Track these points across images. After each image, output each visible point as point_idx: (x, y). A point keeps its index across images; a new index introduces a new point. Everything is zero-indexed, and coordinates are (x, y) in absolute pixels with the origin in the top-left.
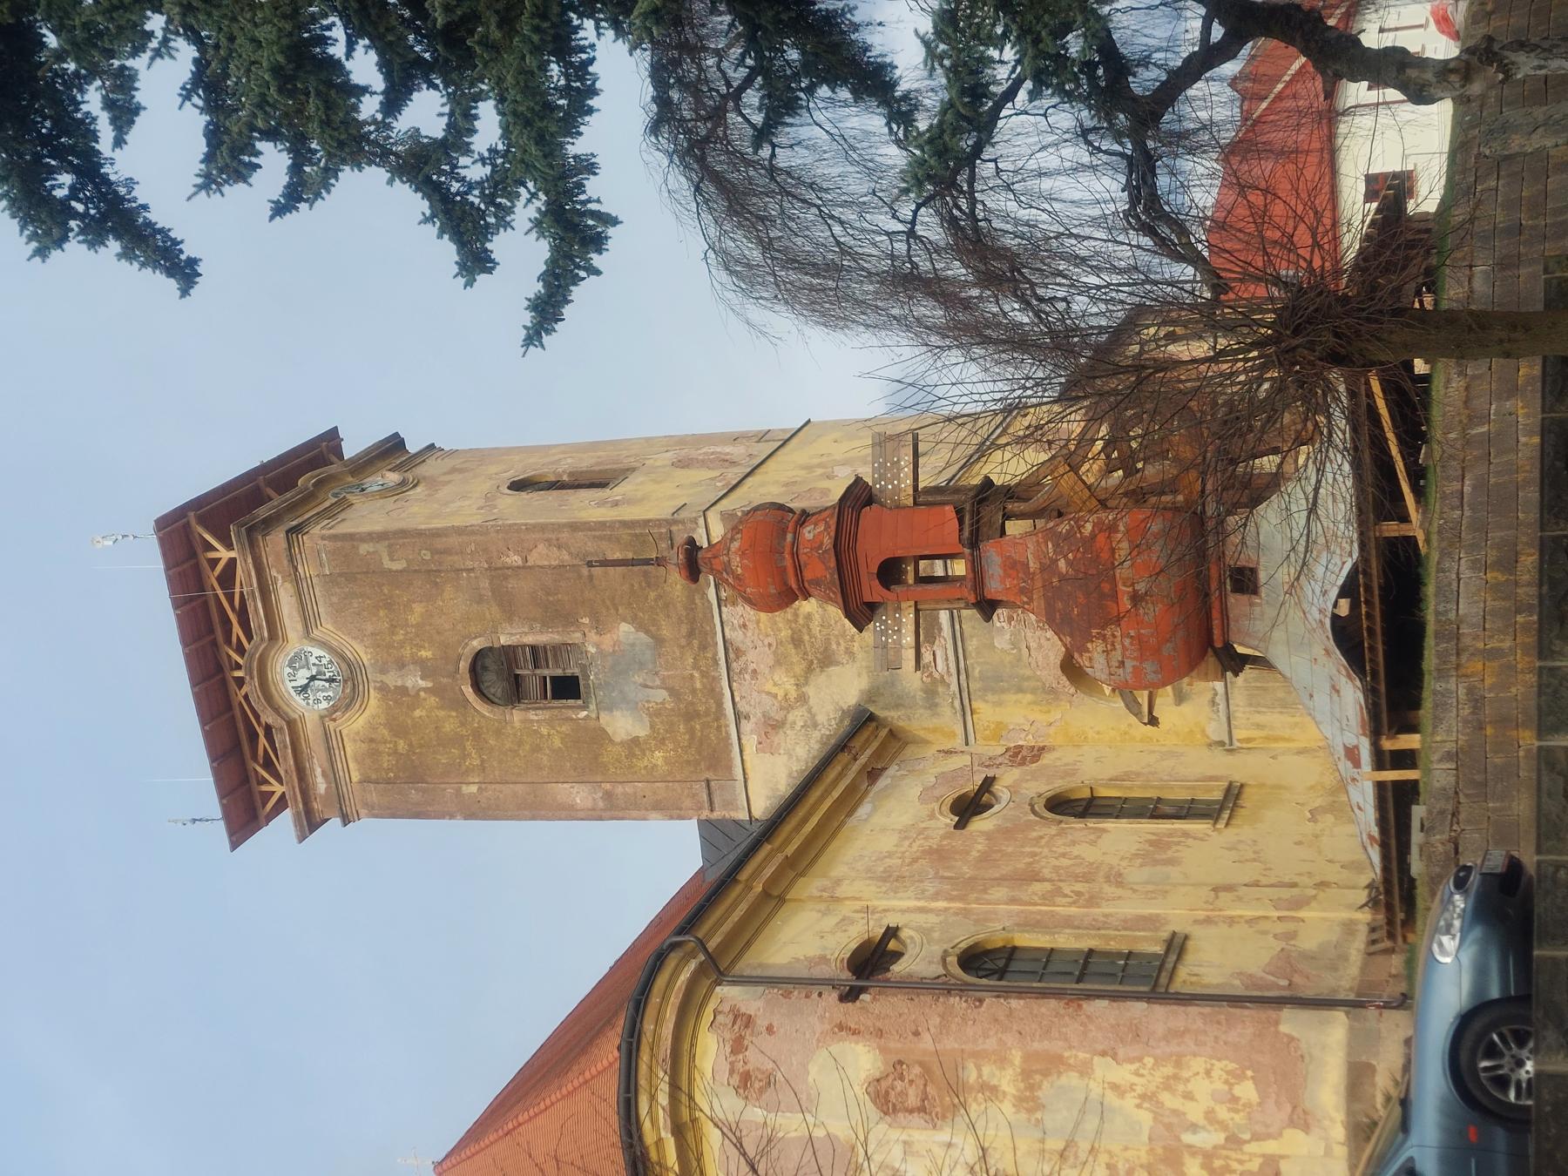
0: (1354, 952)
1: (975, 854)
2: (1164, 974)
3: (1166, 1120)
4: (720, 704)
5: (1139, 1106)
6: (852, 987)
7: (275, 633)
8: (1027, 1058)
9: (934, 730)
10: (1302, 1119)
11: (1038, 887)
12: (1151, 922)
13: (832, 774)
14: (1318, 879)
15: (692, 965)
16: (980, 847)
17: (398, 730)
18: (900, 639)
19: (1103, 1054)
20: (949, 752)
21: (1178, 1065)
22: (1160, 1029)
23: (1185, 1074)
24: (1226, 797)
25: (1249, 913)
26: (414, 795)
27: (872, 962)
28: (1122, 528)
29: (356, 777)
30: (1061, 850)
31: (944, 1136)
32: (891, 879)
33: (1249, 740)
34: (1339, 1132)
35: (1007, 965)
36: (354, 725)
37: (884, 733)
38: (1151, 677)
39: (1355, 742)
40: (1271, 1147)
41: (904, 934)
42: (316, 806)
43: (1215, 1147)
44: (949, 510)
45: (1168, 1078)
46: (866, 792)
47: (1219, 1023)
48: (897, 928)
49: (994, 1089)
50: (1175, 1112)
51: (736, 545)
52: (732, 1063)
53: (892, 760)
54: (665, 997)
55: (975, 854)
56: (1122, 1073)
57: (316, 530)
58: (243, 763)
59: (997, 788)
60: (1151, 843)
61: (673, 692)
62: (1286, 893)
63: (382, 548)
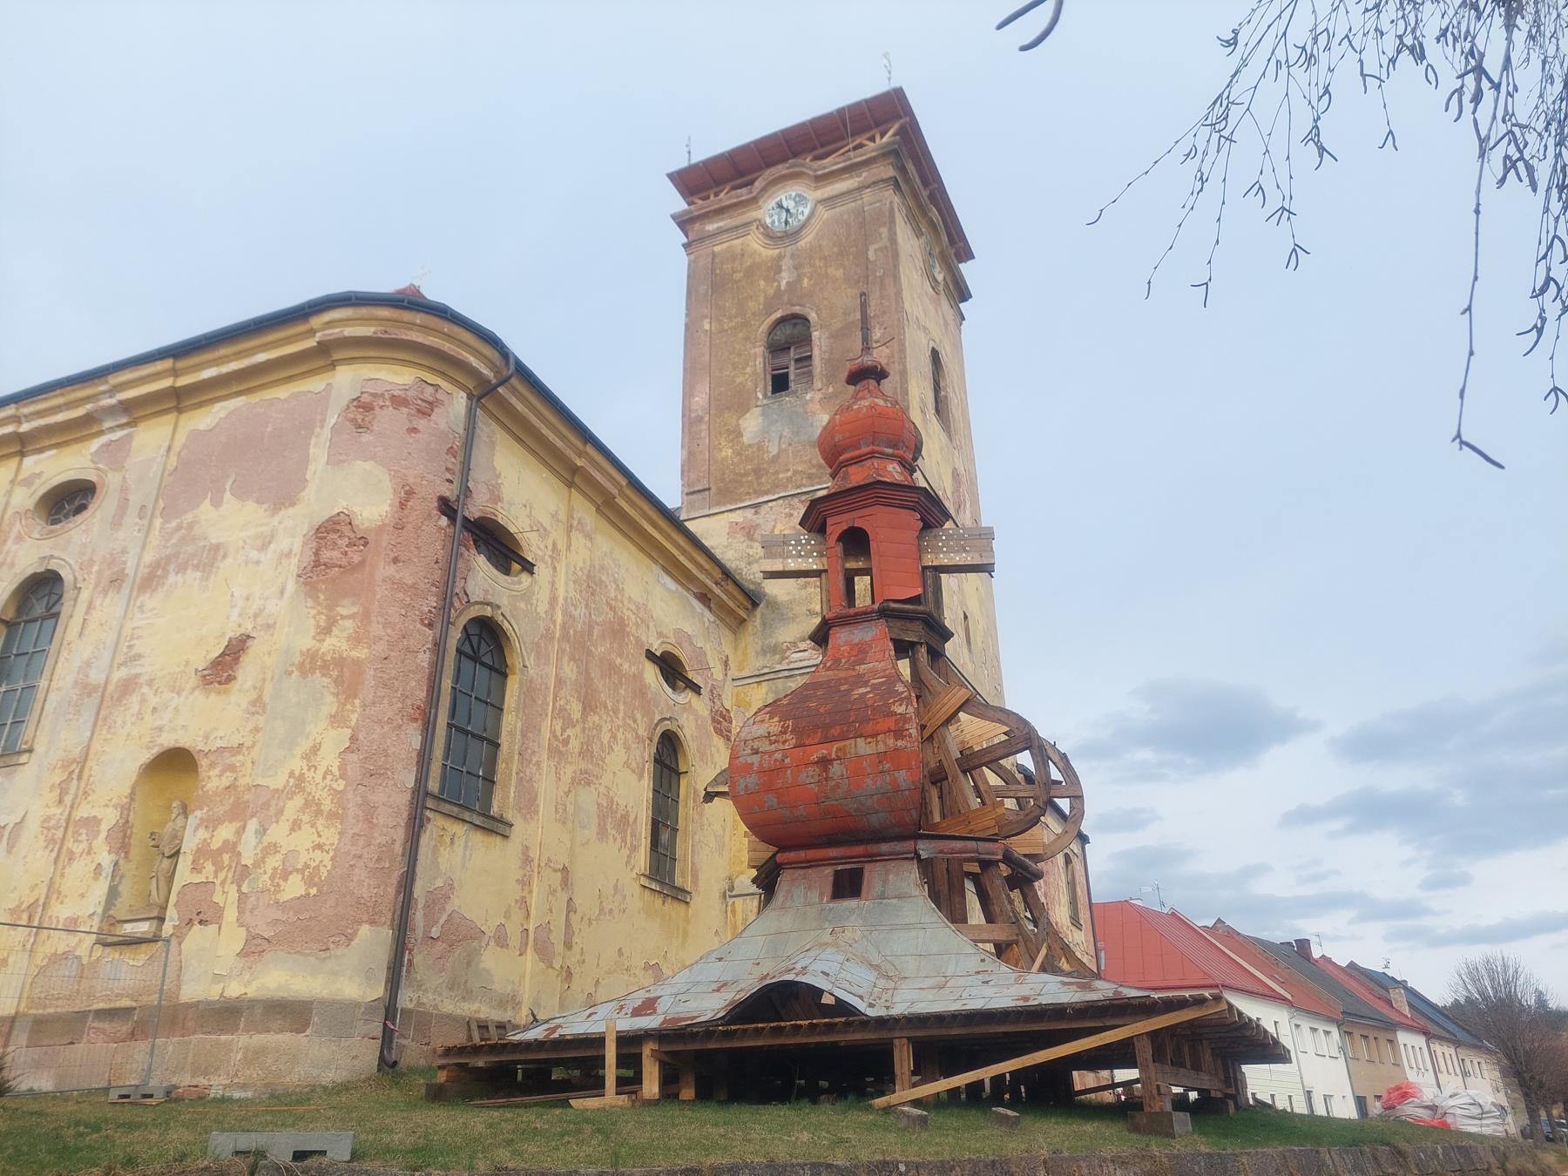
0: (475, 1007)
1: (619, 661)
2: (456, 809)
3: (273, 802)
4: (766, 493)
5: (292, 774)
6: (455, 511)
7: (821, 179)
8: (357, 663)
9: (745, 654)
10: (254, 949)
11: (575, 709)
12: (529, 804)
13: (701, 559)
14: (575, 970)
15: (485, 371)
16: (626, 666)
17: (749, 272)
18: (793, 557)
19: (353, 739)
20: (726, 663)
21: (332, 815)
22: (378, 797)
23: (321, 822)
24: (493, 818)
25: (534, 902)
26: (702, 289)
27: (500, 547)
28: (900, 743)
29: (717, 249)
30: (620, 735)
31: (291, 586)
32: (591, 583)
33: (734, 911)
34: (234, 990)
35: (483, 664)
36: (753, 241)
37: (742, 613)
38: (742, 783)
39: (659, 1011)
40: (231, 914)
41: (525, 577)
42: (697, 226)
43: (239, 854)
44: (920, 591)
45: (319, 804)
46: (688, 589)
47: (379, 860)
48: (532, 573)
49: (326, 631)
50: (281, 811)
51: (880, 402)
52: (382, 395)
53: (718, 616)
54: (449, 337)
55: (619, 661)
56: (329, 758)
57: (897, 199)
58: (732, 179)
59: (688, 696)
60: (625, 817)
61: (778, 456)
62: (557, 937)
63: (885, 242)
